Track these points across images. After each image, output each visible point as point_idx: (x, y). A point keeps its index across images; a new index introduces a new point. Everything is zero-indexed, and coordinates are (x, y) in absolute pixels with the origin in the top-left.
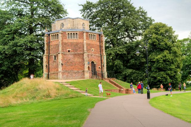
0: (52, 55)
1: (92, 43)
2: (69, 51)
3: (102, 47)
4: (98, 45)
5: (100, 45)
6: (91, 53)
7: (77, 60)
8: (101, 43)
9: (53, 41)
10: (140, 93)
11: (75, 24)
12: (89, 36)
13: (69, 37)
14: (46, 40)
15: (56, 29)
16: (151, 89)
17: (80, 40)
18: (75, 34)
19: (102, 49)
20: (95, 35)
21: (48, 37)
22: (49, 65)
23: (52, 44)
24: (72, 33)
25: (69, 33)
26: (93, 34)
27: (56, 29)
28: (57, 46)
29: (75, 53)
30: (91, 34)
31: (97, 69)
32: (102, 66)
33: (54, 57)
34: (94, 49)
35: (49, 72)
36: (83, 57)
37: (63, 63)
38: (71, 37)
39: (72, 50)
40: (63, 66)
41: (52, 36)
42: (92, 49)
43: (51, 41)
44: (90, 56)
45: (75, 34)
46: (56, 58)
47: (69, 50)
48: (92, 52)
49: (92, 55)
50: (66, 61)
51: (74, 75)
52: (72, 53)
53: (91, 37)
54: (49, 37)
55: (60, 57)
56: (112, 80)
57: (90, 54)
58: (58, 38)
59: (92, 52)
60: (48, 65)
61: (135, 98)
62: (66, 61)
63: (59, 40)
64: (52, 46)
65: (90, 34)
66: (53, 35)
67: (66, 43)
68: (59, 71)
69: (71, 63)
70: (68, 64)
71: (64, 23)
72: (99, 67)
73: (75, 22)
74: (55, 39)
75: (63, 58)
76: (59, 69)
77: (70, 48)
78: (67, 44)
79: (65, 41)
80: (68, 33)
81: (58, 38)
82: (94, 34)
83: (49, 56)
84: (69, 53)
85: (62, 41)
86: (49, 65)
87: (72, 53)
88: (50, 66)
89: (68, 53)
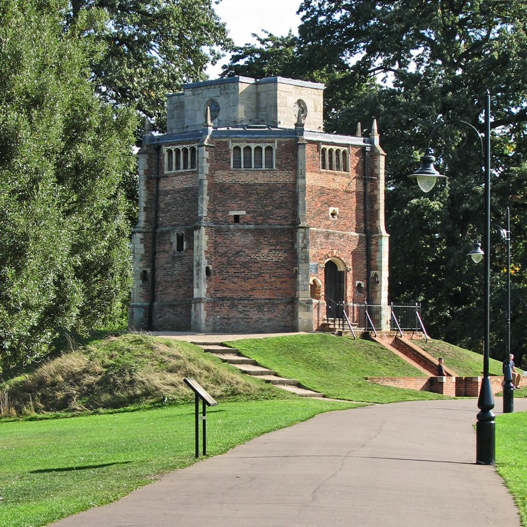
0: (168, 232)
1: (334, 186)
2: (237, 219)
3: (374, 199)
5: (365, 193)
6: (328, 227)
7: (268, 255)
8: (369, 185)
9: (176, 175)
10: (338, 168)
11: (263, 105)
13: (237, 164)
14: (146, 167)
15: (188, 122)
17: (284, 173)
18: (253, 148)
19: (372, 207)
21: (155, 156)
23: (168, 188)
27: (188, 122)
28: (193, 195)
29: (260, 227)
33: (174, 239)
34: (337, 210)
36: (293, 244)
37: (211, 267)
39: (248, 212)
40: (213, 277)
41: (170, 152)
42: (331, 209)
43: (166, 172)
44: (323, 247)
45: (253, 148)
46: (185, 243)
48: (328, 222)
49: (327, 236)
50: (224, 260)
52: (247, 227)
54: (159, 159)
55: (203, 239)
57: (319, 230)
58: (193, 166)
59: (328, 222)
60: (149, 270)
62: (224, 260)
63: (197, 172)
64: (167, 193)
65: (237, 149)
66: (173, 148)
67: (227, 186)
68: (195, 296)
69: (245, 265)
70: (232, 271)
71: (221, 101)
72: (357, 282)
73: (263, 96)
74: (189, 166)
75: (215, 245)
76: (195, 290)
77: (240, 209)
78: (230, 187)
79: (223, 177)
80: (235, 144)
81: (193, 166)
82: (342, 149)
85: (211, 176)
86: (154, 270)
87: (247, 227)
88: (160, 274)
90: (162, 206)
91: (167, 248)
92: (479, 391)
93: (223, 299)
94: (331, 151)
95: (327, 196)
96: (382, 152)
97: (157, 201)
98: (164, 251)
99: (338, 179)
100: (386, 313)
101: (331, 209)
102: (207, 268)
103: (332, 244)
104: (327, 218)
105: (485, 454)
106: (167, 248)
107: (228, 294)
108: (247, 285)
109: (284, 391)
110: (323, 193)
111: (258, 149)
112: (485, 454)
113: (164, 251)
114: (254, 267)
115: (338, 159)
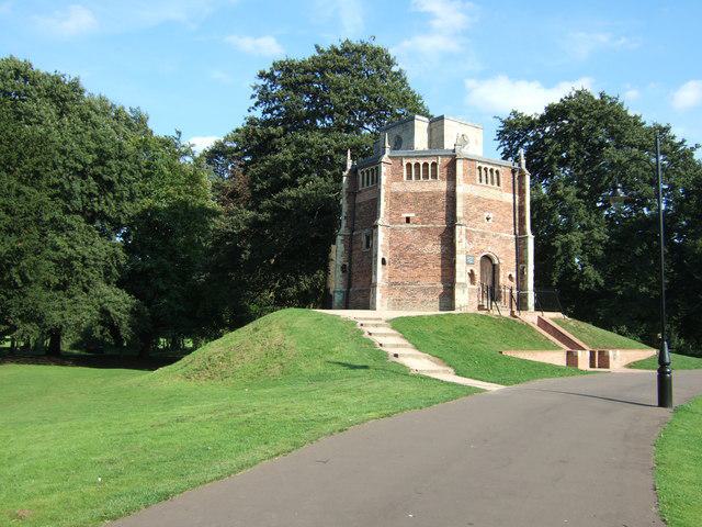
2: (408, 220)
4: (507, 205)
12: (478, 171)
13: (409, 177)
16: (608, 367)
20: (497, 172)
22: (350, 264)
24: (421, 162)
25: (409, 161)
26: (489, 167)
30: (483, 166)
31: (503, 280)
32: (521, 274)
35: (349, 288)
38: (426, 177)
47: (408, 215)
49: (483, 235)
51: (421, 296)
53: (495, 178)
56: (548, 316)
61: (166, 496)
64: (360, 204)
69: (413, 257)
70: (403, 261)
77: (411, 211)
82: (495, 168)
83: (352, 235)
84: (409, 225)
86: (350, 264)
89: (404, 226)
90: (357, 214)
91: (359, 246)
92: (645, 371)
93: (396, 283)
94: (491, 170)
95: (483, 204)
96: (527, 172)
97: (354, 212)
98: (357, 249)
99: (492, 191)
100: (343, 202)
101: (486, 215)
102: (383, 259)
103: (488, 242)
104: (483, 222)
105: (664, 398)
106: (359, 246)
107: (400, 280)
108: (415, 273)
109: (442, 359)
110: (479, 201)
111: (426, 165)
112: (664, 398)
113: (357, 249)
114: (421, 258)
115: (492, 177)
